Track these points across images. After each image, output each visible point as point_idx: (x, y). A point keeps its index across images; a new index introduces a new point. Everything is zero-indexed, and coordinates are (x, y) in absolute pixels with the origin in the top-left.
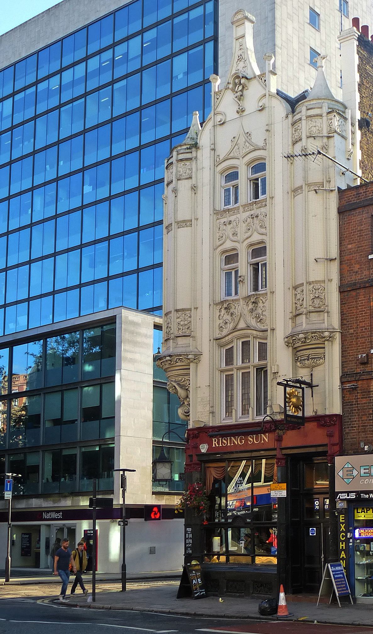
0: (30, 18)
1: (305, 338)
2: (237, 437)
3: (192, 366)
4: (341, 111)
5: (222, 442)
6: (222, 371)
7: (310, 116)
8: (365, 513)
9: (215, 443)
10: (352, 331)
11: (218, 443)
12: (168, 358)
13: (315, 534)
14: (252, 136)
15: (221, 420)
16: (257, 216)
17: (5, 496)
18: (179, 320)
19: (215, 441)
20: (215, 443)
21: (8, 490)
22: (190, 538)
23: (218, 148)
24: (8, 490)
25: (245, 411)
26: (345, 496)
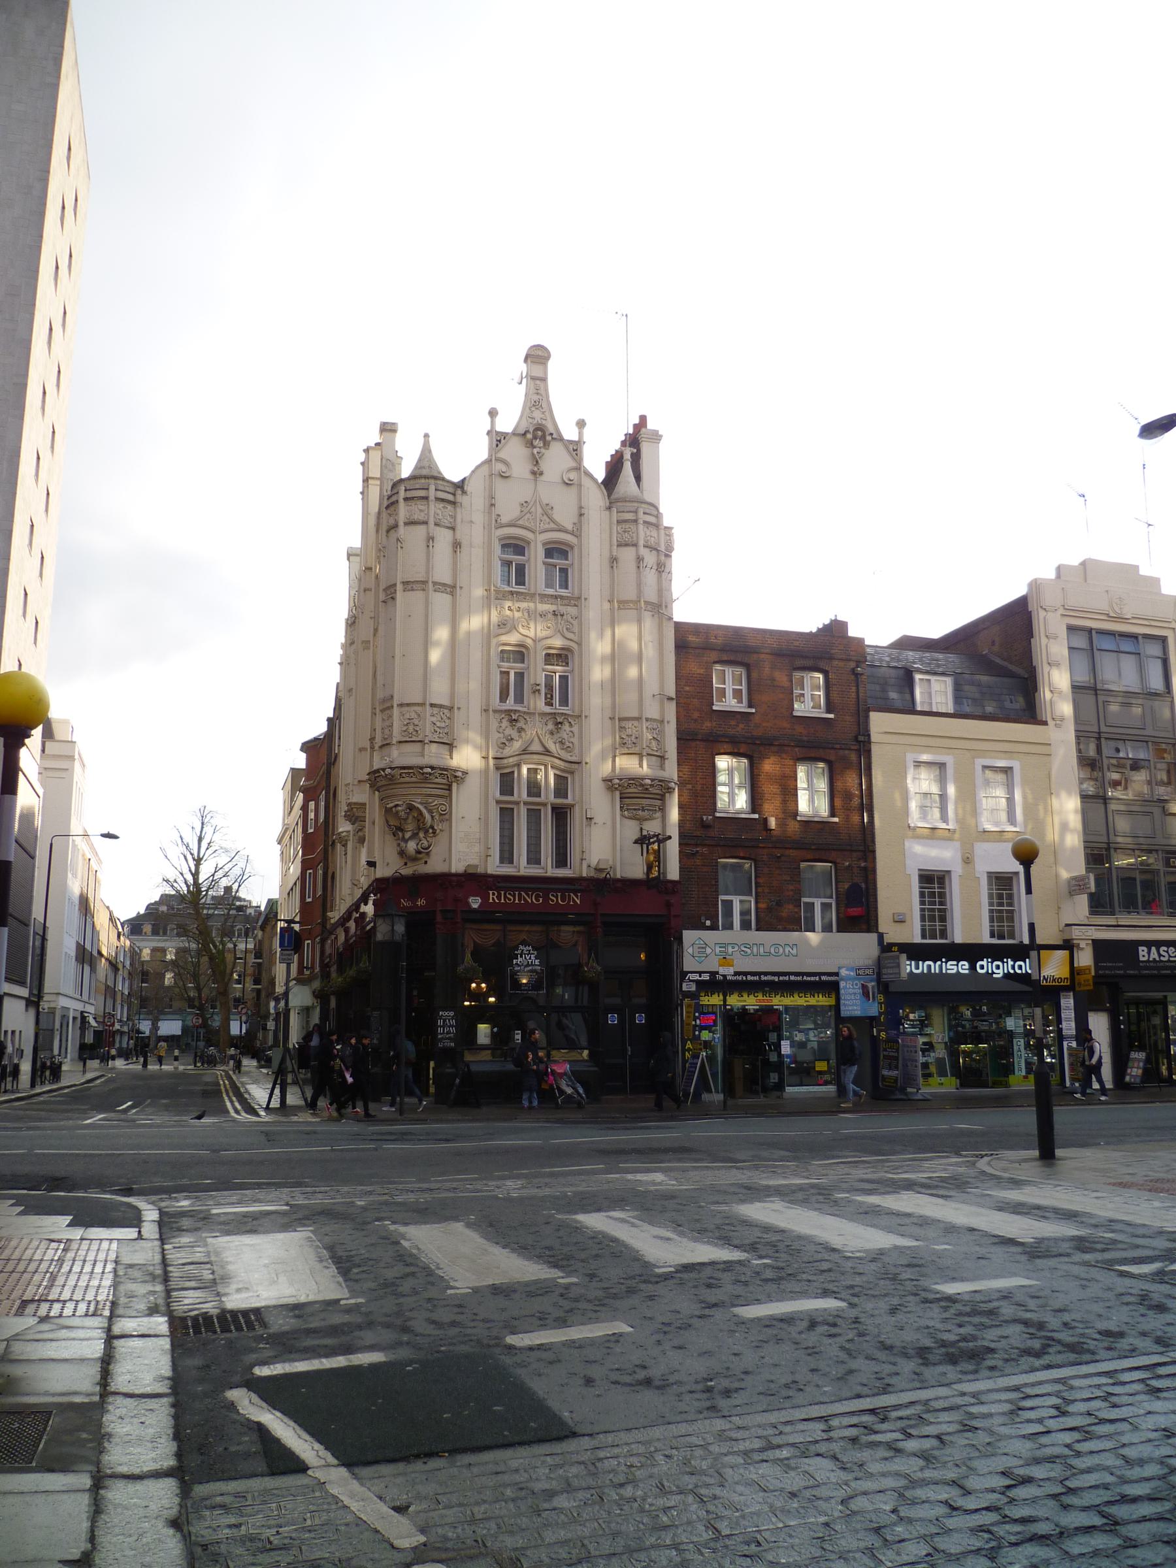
5: (505, 897)
6: (498, 802)
9: (492, 897)
11: (499, 897)
12: (429, 770)
14: (554, 511)
15: (494, 867)
16: (562, 615)
18: (434, 719)
19: (493, 894)
22: (452, 1026)
23: (499, 509)
25: (534, 858)
26: (696, 977)
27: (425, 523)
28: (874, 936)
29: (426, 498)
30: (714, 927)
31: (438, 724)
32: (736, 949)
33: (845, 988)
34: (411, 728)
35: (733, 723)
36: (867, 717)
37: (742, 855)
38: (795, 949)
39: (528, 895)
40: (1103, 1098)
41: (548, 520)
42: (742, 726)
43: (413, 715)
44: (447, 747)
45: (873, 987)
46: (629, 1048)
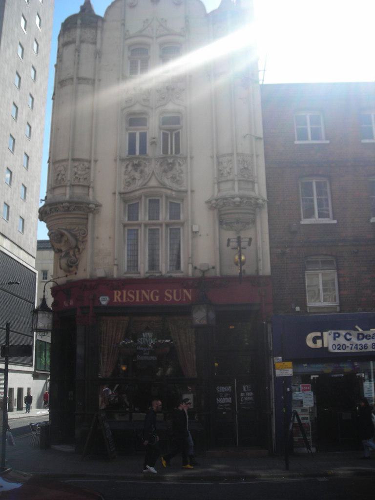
0: (38, 230)
1: (240, 202)
2: (149, 291)
3: (91, 216)
4: (62, 229)
6: (125, 226)
11: (121, 297)
19: (117, 294)
20: (117, 297)
39: (147, 292)
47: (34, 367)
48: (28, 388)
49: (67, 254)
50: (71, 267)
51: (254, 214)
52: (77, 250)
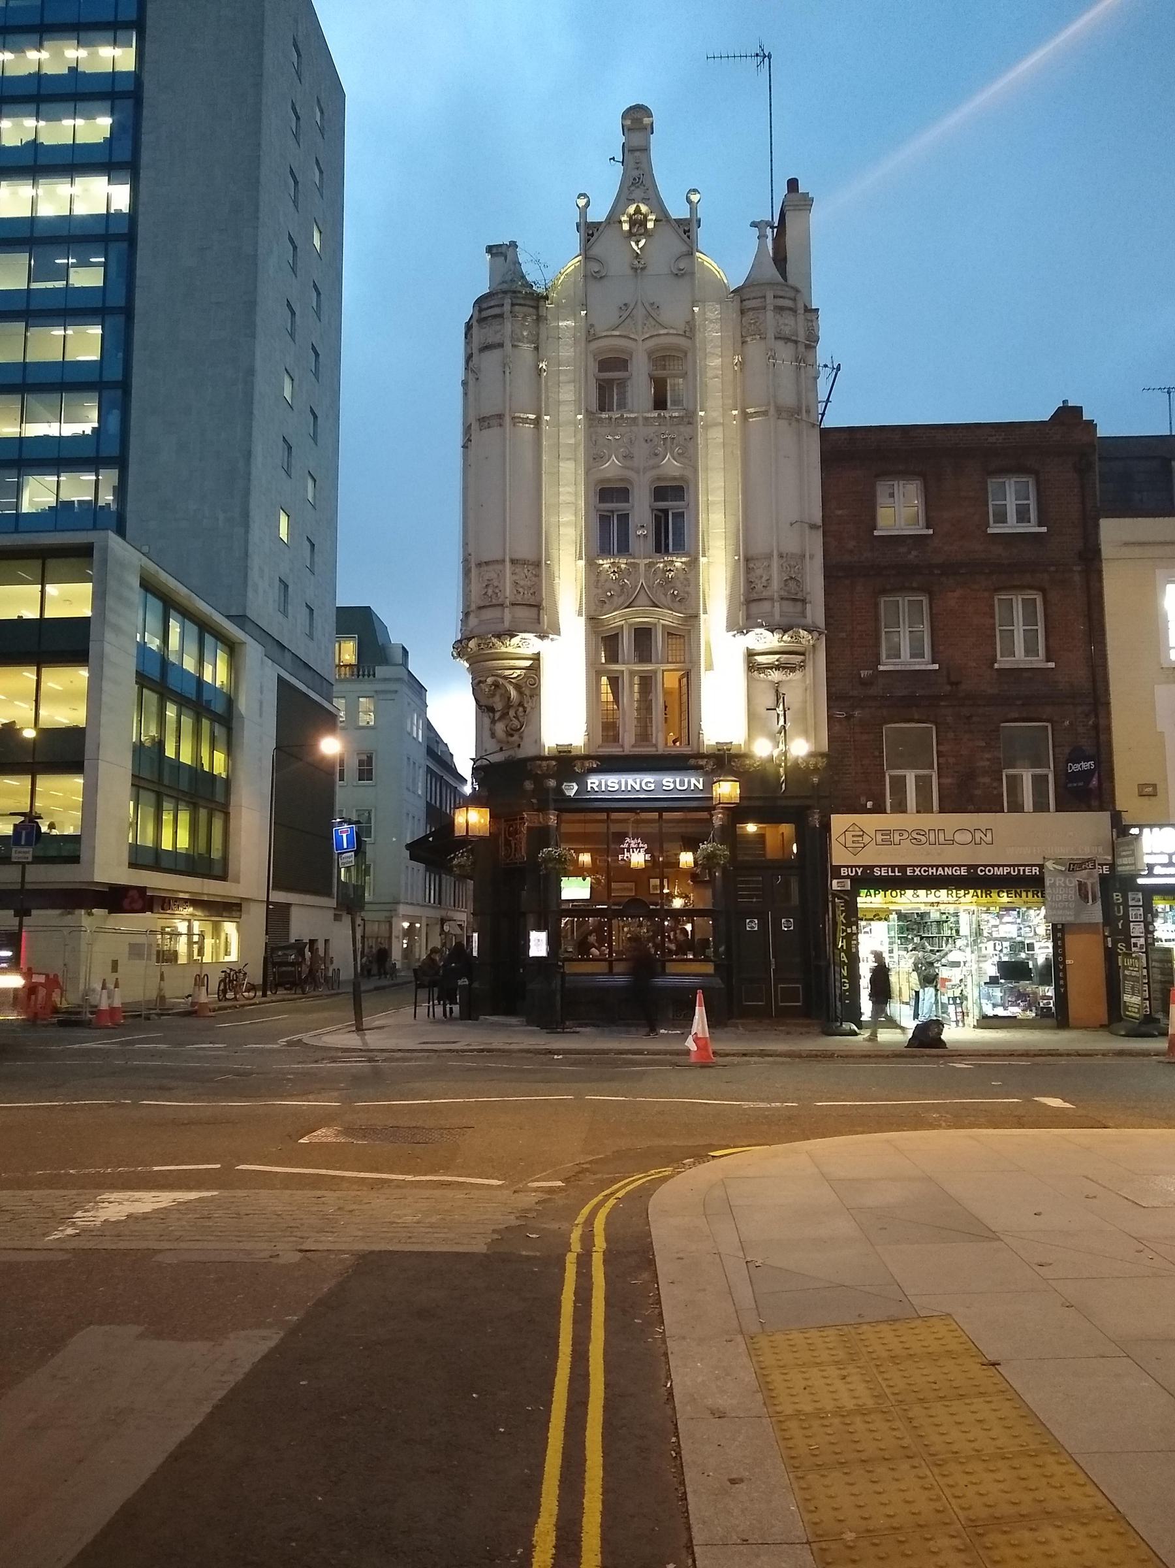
7: (485, 319)
8: (978, 897)
10: (843, 635)
13: (792, 928)
17: (13, 855)
21: (23, 843)
24: (23, 843)
27: (501, 345)
28: (1106, 816)
29: (501, 316)
30: (879, 809)
31: (522, 583)
32: (906, 835)
33: (1053, 885)
34: (490, 592)
35: (903, 550)
36: (1097, 526)
37: (916, 717)
38: (989, 834)
40: (669, 1385)
41: (653, 323)
42: (914, 553)
43: (493, 575)
44: (500, 608)
45: (1092, 884)
46: (773, 960)
47: (335, 900)
48: (113, 961)
49: (504, 715)
50: (512, 735)
51: (772, 616)
52: (521, 709)
